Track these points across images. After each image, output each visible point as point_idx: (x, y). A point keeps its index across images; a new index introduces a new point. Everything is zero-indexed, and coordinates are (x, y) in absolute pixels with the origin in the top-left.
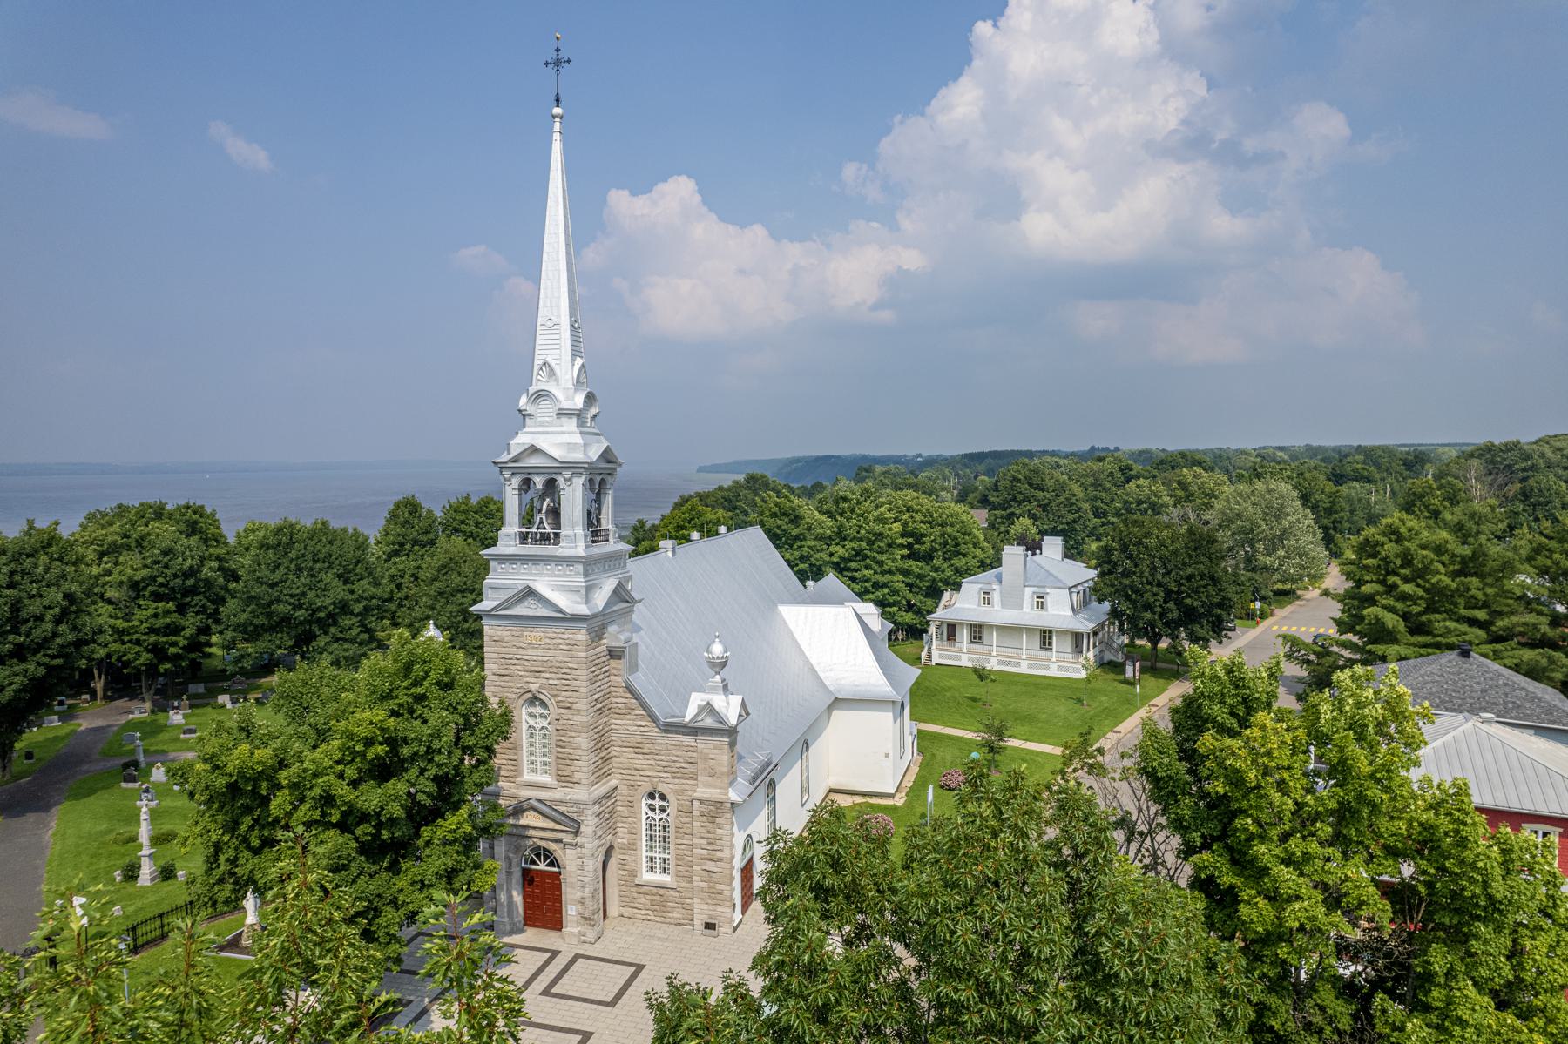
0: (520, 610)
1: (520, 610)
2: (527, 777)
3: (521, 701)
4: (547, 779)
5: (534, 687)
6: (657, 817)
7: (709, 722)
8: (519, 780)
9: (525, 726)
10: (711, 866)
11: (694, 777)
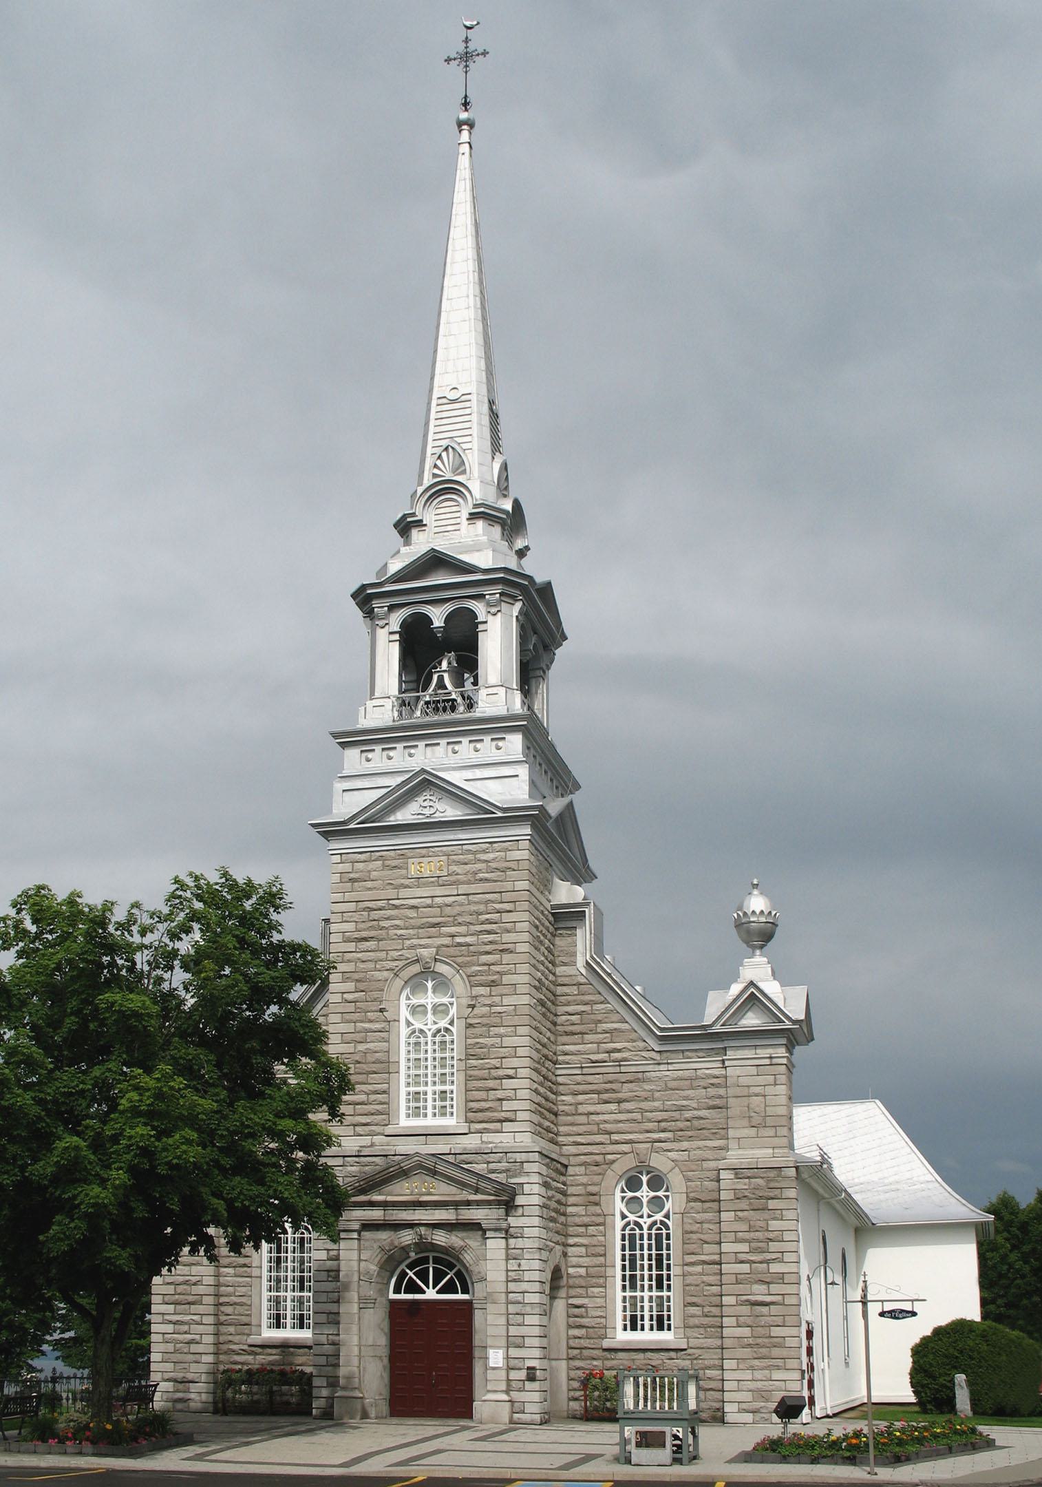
0: (403, 816)
1: (403, 816)
2: (405, 1122)
3: (399, 983)
4: (449, 1123)
5: (426, 953)
6: (646, 1222)
7: (752, 1020)
8: (390, 1130)
9: (404, 1031)
10: (759, 1292)
11: (721, 1131)
